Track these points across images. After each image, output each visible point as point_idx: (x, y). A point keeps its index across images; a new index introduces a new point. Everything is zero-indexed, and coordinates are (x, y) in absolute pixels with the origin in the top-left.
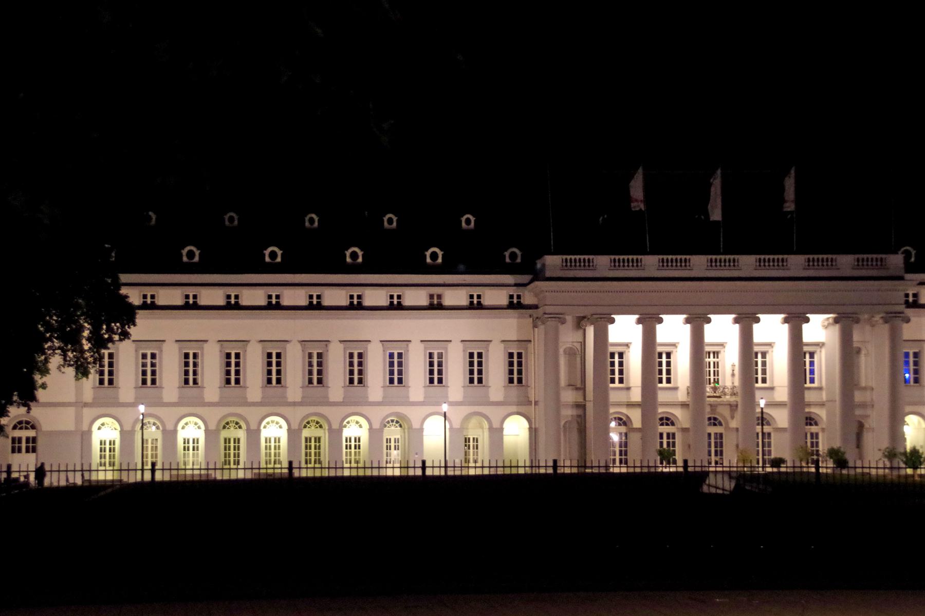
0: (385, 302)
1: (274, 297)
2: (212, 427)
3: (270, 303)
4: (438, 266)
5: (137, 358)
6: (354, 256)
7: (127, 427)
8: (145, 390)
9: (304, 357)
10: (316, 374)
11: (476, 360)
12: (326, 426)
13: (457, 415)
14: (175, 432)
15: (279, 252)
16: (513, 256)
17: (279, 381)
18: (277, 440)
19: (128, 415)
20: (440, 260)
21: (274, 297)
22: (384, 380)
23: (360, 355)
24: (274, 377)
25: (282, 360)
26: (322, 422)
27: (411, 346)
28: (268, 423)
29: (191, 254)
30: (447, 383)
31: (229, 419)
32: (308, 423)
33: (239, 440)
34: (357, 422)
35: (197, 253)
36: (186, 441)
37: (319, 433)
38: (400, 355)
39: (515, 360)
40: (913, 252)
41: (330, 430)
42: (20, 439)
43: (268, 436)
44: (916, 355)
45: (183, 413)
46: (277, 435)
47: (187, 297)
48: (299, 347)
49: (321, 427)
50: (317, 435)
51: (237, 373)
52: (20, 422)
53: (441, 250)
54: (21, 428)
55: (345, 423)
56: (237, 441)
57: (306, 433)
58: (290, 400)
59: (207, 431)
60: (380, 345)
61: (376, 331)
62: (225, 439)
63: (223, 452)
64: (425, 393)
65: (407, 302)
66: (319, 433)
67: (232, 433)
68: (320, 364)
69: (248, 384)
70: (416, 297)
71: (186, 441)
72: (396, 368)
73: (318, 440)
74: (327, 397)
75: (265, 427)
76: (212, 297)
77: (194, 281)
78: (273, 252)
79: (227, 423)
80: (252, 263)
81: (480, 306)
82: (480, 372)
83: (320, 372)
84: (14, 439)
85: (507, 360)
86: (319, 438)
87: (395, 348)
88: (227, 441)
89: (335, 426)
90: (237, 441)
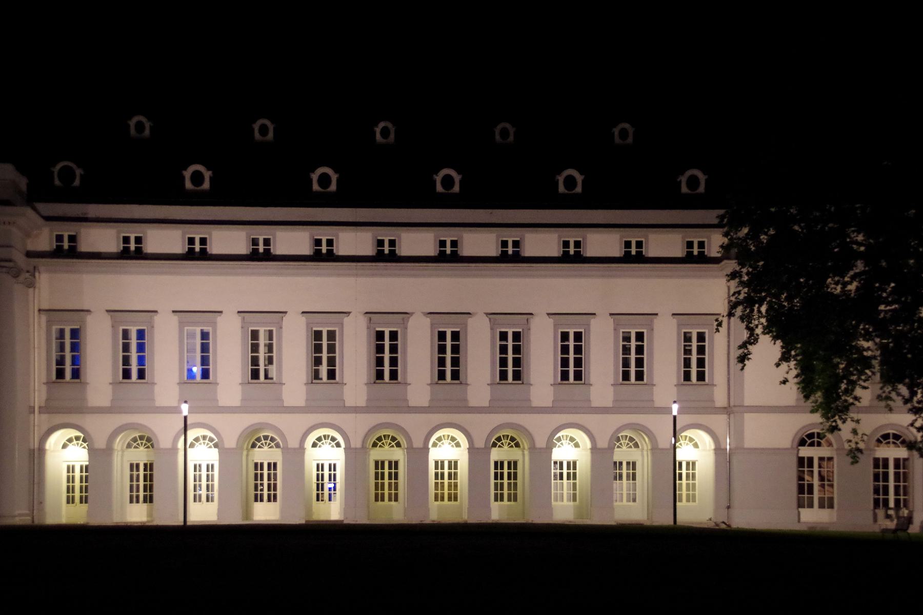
0: (431, 250)
1: (386, 244)
2: (356, 443)
3: (191, 251)
4: (204, 192)
5: (493, 337)
6: (448, 182)
7: (101, 444)
8: (503, 388)
9: (244, 338)
10: (511, 362)
11: (449, 343)
12: (525, 444)
13: (233, 427)
14: (426, 450)
15: (207, 175)
16: (570, 182)
17: (394, 375)
18: (454, 464)
19: (101, 426)
20: (456, 189)
21: (386, 244)
22: (493, 375)
23: (456, 336)
24: (387, 369)
25: (461, 343)
26: (400, 438)
27: (657, 323)
28: (439, 439)
29: (197, 178)
30: (405, 378)
31: (501, 434)
32: (258, 440)
33: (396, 463)
34: (572, 439)
35: (334, 177)
36: (439, 464)
37: (398, 455)
38: (517, 336)
39: (449, 343)
40: (79, 172)
41: (533, 448)
42: (886, 461)
43: (439, 457)
44: (517, 336)
45: (445, 421)
46: (453, 457)
47: (126, 240)
48: (237, 321)
49: (636, 445)
50: (512, 458)
51: (394, 362)
52: (811, 436)
53: (336, 172)
54: (812, 444)
55: (433, 439)
56: (394, 465)
57: (496, 454)
58: (349, 403)
59: (472, 450)
60: (611, 320)
61: (479, 297)
62: (377, 463)
63: (372, 481)
64: (432, 393)
65: (215, 248)
66: (398, 455)
67: (264, 455)
68: (456, 349)
69: (409, 380)
70: (165, 240)
71: (320, 467)
72: (449, 356)
73: (513, 465)
74: (466, 400)
75: (435, 445)
76: (603, 243)
77: (137, 215)
78: (196, 173)
79: (379, 439)
80: (302, 196)
81: (331, 257)
82: (578, 363)
83: (517, 362)
84: (876, 462)
85: (374, 342)
86: (515, 463)
87: (693, 326)
88: (379, 464)
89: (541, 443)
90: (394, 465)
